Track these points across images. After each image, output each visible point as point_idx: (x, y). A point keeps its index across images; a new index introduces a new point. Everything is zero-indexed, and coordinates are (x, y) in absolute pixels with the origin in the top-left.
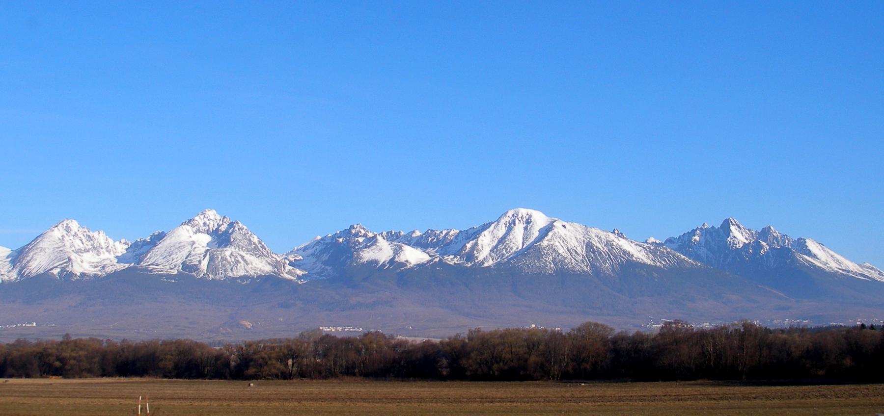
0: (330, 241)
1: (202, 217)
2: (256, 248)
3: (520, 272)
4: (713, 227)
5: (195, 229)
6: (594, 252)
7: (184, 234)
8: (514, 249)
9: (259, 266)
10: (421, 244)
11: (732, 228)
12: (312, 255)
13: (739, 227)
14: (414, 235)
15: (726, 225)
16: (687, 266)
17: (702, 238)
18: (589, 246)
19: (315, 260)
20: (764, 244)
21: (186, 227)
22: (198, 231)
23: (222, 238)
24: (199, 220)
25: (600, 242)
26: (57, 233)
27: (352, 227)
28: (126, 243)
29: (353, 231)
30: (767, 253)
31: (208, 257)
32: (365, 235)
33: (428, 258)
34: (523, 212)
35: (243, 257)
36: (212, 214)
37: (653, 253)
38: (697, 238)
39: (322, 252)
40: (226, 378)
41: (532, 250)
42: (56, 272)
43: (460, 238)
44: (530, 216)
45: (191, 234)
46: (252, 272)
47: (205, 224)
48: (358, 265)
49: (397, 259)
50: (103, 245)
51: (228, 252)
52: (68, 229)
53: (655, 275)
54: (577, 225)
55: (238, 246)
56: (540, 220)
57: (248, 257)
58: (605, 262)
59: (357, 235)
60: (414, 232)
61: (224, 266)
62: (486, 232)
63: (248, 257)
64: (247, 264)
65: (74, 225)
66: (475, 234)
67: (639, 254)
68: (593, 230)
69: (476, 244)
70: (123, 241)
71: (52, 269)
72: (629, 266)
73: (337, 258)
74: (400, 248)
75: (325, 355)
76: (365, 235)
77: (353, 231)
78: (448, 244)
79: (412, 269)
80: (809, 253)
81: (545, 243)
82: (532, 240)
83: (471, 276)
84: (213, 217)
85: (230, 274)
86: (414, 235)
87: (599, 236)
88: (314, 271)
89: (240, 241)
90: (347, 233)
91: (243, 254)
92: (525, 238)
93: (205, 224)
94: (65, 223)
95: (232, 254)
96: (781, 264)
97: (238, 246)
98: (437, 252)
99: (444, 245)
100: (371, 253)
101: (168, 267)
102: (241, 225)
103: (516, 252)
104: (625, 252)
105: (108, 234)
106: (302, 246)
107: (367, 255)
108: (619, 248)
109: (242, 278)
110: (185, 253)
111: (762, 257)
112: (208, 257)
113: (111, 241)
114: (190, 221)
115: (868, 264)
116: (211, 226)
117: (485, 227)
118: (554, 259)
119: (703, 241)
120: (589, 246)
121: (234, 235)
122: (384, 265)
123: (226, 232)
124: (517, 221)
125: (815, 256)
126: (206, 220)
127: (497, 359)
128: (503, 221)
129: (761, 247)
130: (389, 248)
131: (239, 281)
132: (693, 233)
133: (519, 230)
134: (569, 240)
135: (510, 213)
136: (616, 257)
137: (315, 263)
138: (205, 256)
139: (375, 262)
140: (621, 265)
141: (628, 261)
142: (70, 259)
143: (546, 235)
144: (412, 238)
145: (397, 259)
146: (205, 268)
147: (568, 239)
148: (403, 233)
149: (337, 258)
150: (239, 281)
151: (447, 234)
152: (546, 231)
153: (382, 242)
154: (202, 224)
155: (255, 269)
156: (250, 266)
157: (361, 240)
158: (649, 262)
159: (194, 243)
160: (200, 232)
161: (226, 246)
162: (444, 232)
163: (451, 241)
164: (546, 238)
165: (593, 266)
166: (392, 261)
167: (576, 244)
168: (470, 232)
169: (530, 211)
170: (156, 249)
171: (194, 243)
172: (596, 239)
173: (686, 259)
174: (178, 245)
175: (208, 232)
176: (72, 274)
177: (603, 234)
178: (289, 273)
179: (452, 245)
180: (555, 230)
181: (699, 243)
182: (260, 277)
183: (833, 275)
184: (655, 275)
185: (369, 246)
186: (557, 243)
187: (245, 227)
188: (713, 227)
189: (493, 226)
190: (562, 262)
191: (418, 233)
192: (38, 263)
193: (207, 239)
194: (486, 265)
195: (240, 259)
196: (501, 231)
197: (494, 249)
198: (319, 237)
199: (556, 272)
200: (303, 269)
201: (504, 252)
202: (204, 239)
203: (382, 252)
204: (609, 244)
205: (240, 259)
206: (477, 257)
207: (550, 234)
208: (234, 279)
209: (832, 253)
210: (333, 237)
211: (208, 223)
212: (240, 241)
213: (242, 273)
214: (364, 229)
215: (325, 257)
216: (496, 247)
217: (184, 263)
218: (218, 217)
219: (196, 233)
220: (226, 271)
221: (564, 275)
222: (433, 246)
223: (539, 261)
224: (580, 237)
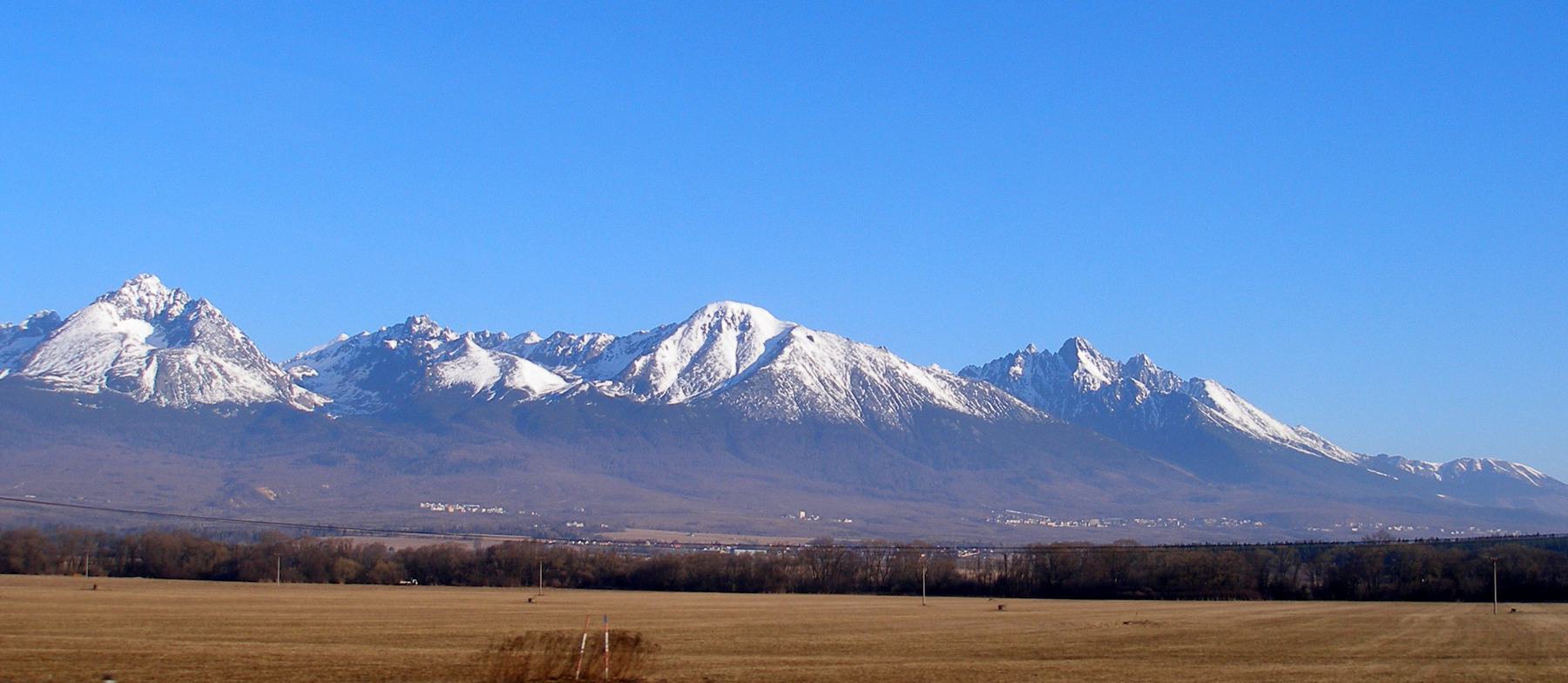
0: (368, 344)
1: (135, 288)
2: (242, 353)
3: (741, 419)
4: (1046, 352)
5: (122, 311)
6: (865, 386)
7: (104, 318)
8: (723, 374)
9: (251, 385)
10: (544, 356)
11: (1082, 355)
12: (336, 368)
13: (1093, 354)
14: (528, 341)
15: (1070, 349)
16: (1027, 418)
17: (1028, 372)
18: (857, 375)
19: (341, 377)
20: (1140, 384)
21: (106, 305)
22: (128, 314)
23: (175, 330)
24: (130, 294)
25: (876, 368)
27: (412, 320)
29: (416, 328)
30: (1147, 401)
31: (154, 363)
32: (442, 337)
33: (564, 384)
34: (734, 308)
35: (220, 367)
36: (152, 283)
37: (967, 391)
38: (1018, 369)
39: (354, 364)
40: (730, 591)
41: (756, 378)
43: (616, 350)
44: (748, 317)
45: (116, 319)
46: (239, 396)
47: (140, 301)
48: (436, 391)
49: (508, 384)
51: (192, 355)
53: (976, 432)
54: (832, 337)
55: (210, 345)
56: (766, 325)
57: (228, 367)
58: (886, 404)
59: (425, 335)
60: (527, 335)
61: (186, 381)
62: (668, 342)
63: (228, 367)
64: (230, 381)
66: (649, 343)
67: (944, 395)
68: (862, 346)
69: (653, 362)
72: (928, 414)
73: (390, 378)
74: (513, 363)
75: (1337, 561)
76: (442, 337)
77: (416, 328)
78: (595, 360)
79: (539, 403)
80: (1212, 403)
81: (779, 366)
82: (753, 359)
83: (644, 418)
85: (198, 397)
86: (528, 341)
87: (873, 359)
88: (341, 399)
89: (213, 336)
90: (404, 330)
91: (221, 361)
92: (741, 356)
93: (140, 301)
95: (199, 361)
96: (1170, 424)
97: (210, 345)
98: (575, 372)
99: (586, 361)
100: (459, 370)
101: (79, 380)
102: (210, 307)
103: (726, 380)
107: (451, 374)
109: (225, 406)
110: (110, 353)
111: (1138, 408)
112: (154, 363)
114: (112, 295)
115: (1304, 429)
116: (153, 306)
117: (670, 330)
118: (797, 397)
119: (1029, 375)
120: (857, 375)
121: (200, 326)
122: (484, 392)
123: (183, 318)
124: (724, 324)
125: (1221, 410)
126: (143, 294)
127: (1133, 573)
128: (698, 323)
129: (1138, 391)
130: (491, 361)
131: (217, 411)
132: (1011, 360)
133: (728, 341)
134: (820, 363)
135: (712, 309)
137: (341, 384)
138: (149, 362)
139: (466, 387)
140: (915, 411)
141: (925, 404)
143: (781, 352)
144: (525, 347)
145: (508, 384)
146: (152, 385)
147: (819, 361)
148: (506, 336)
149: (390, 378)
150: (217, 411)
151: (593, 341)
152: (778, 345)
153: (476, 352)
154: (135, 303)
155: (244, 389)
156: (234, 384)
157: (435, 344)
158: (961, 408)
159: (125, 336)
160: (132, 316)
161: (185, 344)
162: (587, 338)
164: (781, 358)
165: (865, 411)
166: (500, 386)
167: (834, 371)
168: (635, 340)
169: (747, 308)
170: (51, 345)
171: (125, 336)
172: (868, 363)
173: (1024, 405)
174: (94, 340)
175: (146, 317)
177: (879, 356)
178: (301, 399)
179: (602, 362)
180: (796, 344)
181: (1022, 378)
182: (254, 405)
183: (1262, 444)
184: (976, 432)
185: (453, 358)
186: (800, 368)
187: (218, 312)
188: (1046, 352)
189: (680, 330)
191: (535, 338)
193: (146, 329)
194: (674, 401)
195: (215, 370)
196: (697, 341)
197: (686, 373)
198: (345, 337)
199: (803, 417)
200: (324, 395)
201: (704, 378)
202: (140, 330)
203: (480, 369)
204: (889, 372)
205: (215, 370)
206: (655, 387)
207: (787, 350)
208: (207, 408)
209: (1250, 407)
210: (374, 337)
211: (146, 299)
212: (213, 336)
213: (220, 397)
214: (437, 323)
215: (362, 373)
216: (689, 369)
217: (109, 374)
218: (166, 292)
219: (123, 317)
220: (190, 391)
221: (816, 427)
222: (568, 362)
223: (771, 398)
224: (840, 358)
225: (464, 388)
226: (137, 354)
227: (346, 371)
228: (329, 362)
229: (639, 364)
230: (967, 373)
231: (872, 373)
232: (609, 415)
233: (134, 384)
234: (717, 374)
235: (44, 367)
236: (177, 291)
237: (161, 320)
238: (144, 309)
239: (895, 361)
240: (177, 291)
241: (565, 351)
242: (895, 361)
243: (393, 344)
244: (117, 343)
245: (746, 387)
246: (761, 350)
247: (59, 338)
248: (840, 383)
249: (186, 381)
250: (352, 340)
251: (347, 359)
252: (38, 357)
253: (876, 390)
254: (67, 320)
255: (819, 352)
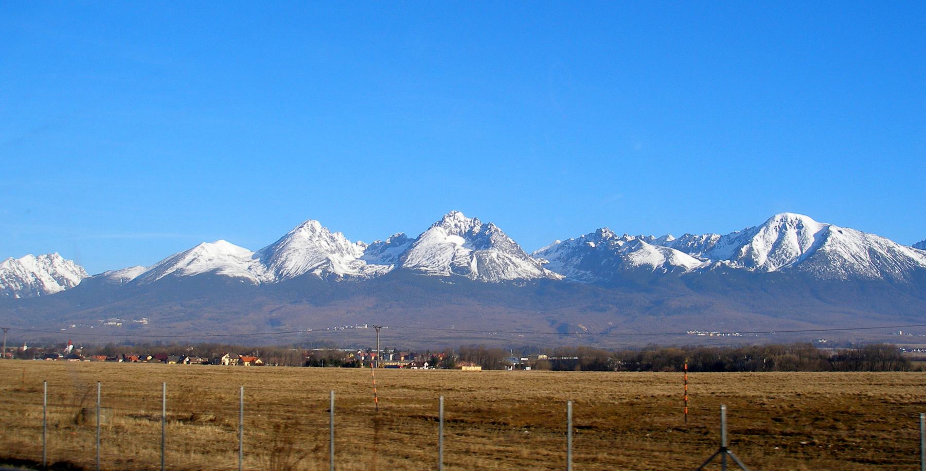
0: (575, 245)
3: (809, 275)
5: (447, 231)
6: (878, 258)
7: (439, 235)
8: (794, 254)
9: (527, 269)
10: (684, 245)
12: (559, 258)
14: (668, 240)
18: (872, 252)
19: (563, 264)
21: (438, 228)
22: (451, 233)
23: (479, 240)
24: (449, 221)
25: (882, 248)
26: (305, 233)
28: (362, 245)
31: (475, 259)
34: (791, 216)
35: (510, 260)
36: (460, 215)
39: (569, 256)
41: (816, 253)
42: (318, 272)
44: (800, 221)
47: (456, 225)
50: (344, 247)
51: (494, 253)
52: (313, 230)
54: (852, 231)
55: (501, 248)
56: (812, 227)
57: (514, 259)
60: (667, 236)
61: (494, 268)
62: (757, 237)
64: (517, 267)
65: (317, 225)
66: (747, 236)
69: (751, 249)
70: (360, 243)
71: (313, 269)
74: (671, 252)
78: (712, 249)
81: (827, 248)
82: (809, 245)
83: (752, 281)
84: (462, 219)
85: (503, 277)
86: (668, 240)
87: (881, 243)
90: (597, 236)
91: (509, 256)
92: (801, 244)
93: (456, 225)
94: (309, 223)
97: (501, 248)
100: (640, 257)
104: (910, 259)
105: (347, 236)
106: (542, 250)
107: (637, 259)
108: (902, 254)
109: (519, 280)
110: (449, 254)
112: (475, 259)
113: (349, 242)
116: (463, 228)
117: (757, 231)
118: (842, 266)
120: (872, 252)
123: (481, 234)
124: (788, 226)
128: (772, 226)
133: (791, 234)
135: (778, 217)
136: (902, 263)
138: (472, 258)
140: (910, 271)
141: (915, 267)
142: (328, 260)
146: (476, 270)
147: (848, 244)
149: (598, 265)
151: (708, 238)
152: (823, 236)
155: (525, 271)
157: (621, 243)
158: (698, 263)
161: (488, 247)
162: (705, 237)
163: (714, 246)
164: (827, 244)
165: (882, 273)
166: (667, 264)
167: (858, 250)
168: (732, 237)
169: (799, 216)
175: (460, 234)
176: (335, 275)
179: (715, 250)
185: (635, 250)
189: (762, 230)
190: (852, 268)
192: (295, 262)
193: (460, 241)
196: (774, 237)
198: (559, 242)
199: (849, 276)
201: (783, 256)
203: (652, 256)
204: (890, 250)
207: (829, 239)
208: (509, 282)
210: (578, 241)
215: (576, 261)
218: (469, 220)
219: (448, 235)
220: (498, 273)
223: (829, 267)
225: (646, 267)
226: (463, 254)
227: (567, 260)
228: (554, 255)
229: (744, 250)
230: (373, 247)
231: (880, 251)
232: (728, 276)
233: (467, 270)
234: (791, 254)
235: (415, 263)
236: (475, 219)
237: (468, 235)
238: (458, 230)
239: (891, 244)
240: (475, 219)
241: (692, 245)
242: (891, 244)
243: (592, 244)
244: (451, 248)
245: (812, 261)
246: (812, 240)
247: (418, 247)
248: (864, 257)
249: (494, 268)
250: (565, 243)
251: (565, 253)
252: (409, 257)
253: (885, 260)
254: (419, 238)
255: (847, 240)
